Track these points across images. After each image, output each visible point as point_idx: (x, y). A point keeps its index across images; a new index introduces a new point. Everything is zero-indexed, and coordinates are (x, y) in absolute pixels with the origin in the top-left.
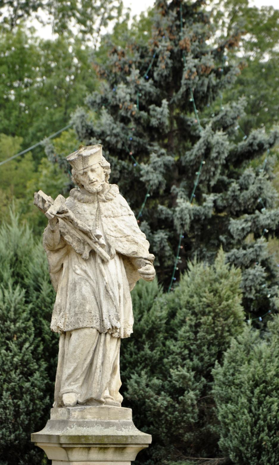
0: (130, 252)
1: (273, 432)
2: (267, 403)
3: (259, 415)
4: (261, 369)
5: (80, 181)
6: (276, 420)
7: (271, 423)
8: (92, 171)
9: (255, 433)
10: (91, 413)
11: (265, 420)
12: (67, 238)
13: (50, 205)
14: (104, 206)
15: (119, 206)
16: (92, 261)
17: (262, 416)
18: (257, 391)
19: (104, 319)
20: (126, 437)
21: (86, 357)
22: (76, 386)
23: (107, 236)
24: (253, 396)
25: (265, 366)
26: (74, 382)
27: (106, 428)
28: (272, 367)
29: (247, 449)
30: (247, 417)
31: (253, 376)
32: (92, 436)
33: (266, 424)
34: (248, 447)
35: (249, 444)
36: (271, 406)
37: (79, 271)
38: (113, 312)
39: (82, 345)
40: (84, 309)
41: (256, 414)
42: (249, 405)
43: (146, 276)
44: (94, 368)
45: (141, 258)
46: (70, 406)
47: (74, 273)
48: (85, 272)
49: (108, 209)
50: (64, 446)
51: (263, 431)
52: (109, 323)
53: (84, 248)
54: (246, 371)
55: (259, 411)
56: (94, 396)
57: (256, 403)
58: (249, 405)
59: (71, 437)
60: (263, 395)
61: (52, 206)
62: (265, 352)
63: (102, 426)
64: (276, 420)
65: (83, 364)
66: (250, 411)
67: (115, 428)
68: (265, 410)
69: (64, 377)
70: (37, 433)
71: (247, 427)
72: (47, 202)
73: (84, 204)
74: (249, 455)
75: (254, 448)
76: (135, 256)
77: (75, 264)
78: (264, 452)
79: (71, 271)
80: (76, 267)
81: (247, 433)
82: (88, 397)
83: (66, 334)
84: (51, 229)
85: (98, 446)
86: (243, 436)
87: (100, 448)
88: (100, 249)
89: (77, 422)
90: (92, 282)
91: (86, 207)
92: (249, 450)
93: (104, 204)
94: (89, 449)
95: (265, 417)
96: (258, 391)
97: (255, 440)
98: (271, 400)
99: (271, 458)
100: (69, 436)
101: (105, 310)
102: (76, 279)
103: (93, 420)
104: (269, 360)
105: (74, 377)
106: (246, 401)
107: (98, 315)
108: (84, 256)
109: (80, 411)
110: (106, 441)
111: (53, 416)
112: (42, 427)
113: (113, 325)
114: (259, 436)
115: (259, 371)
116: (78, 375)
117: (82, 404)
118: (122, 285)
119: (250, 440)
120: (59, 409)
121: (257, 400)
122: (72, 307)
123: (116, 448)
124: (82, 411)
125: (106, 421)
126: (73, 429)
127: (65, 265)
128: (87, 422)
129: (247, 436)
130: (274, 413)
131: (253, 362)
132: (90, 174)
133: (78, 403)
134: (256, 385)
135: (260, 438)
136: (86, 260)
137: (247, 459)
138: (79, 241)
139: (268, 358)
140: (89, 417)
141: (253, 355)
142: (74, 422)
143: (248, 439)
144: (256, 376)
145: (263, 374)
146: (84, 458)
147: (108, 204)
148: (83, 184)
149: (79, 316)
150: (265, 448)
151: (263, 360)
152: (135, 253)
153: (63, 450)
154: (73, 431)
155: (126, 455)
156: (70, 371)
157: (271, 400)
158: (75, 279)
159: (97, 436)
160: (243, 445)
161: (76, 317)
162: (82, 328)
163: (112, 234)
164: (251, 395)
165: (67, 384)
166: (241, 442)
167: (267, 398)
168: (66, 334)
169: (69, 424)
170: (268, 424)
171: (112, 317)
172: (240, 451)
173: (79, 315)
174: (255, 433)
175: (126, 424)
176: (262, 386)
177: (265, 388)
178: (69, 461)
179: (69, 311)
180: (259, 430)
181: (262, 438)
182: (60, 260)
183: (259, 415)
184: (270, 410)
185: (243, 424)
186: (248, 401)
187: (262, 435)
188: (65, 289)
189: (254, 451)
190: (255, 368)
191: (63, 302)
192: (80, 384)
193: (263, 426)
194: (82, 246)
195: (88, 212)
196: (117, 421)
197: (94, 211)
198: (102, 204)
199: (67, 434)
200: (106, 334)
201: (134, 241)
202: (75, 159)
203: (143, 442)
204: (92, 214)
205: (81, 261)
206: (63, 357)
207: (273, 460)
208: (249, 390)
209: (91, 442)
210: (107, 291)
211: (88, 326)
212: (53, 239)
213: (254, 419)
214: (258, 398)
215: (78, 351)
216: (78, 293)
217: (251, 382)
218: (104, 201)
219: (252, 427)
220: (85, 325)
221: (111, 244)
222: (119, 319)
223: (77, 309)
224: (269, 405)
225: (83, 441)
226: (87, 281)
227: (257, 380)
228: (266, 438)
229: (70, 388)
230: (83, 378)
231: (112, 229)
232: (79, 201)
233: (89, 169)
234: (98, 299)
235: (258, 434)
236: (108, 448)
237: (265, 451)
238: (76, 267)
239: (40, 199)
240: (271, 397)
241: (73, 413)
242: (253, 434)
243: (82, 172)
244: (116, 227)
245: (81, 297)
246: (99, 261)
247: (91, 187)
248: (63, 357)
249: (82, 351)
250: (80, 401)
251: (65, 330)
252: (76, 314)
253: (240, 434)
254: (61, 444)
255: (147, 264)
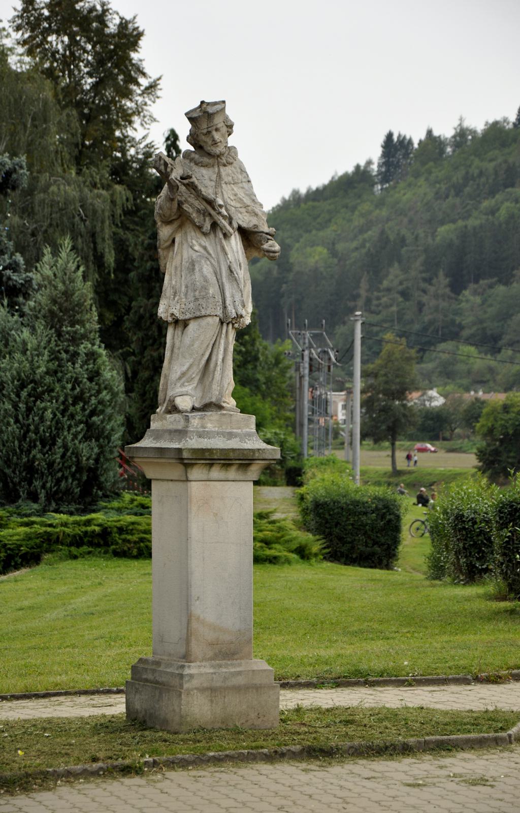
0: (251, 225)
1: (47, 448)
2: (39, 409)
3: (29, 425)
4: (28, 365)
5: (198, 141)
6: (51, 431)
7: (45, 435)
8: (217, 130)
9: (25, 449)
10: (211, 421)
11: (36, 432)
12: (186, 207)
13: (172, 169)
14: (225, 171)
15: (239, 171)
16: (212, 236)
17: (32, 427)
18: (24, 394)
19: (227, 305)
20: (253, 451)
21: (205, 352)
22: (190, 388)
23: (228, 206)
24: (20, 401)
25: (32, 361)
26: (188, 382)
27: (228, 439)
28: (41, 362)
29: (14, 472)
30: (13, 428)
31: (18, 373)
32: (216, 449)
33: (38, 438)
34: (15, 469)
35: (17, 464)
36: (43, 413)
37: (197, 248)
38: (238, 298)
39: (202, 338)
40: (207, 293)
41: (24, 424)
42: (15, 413)
43: (271, 254)
44: (212, 365)
45: (263, 232)
46: (187, 412)
47: (190, 250)
48: (205, 248)
49: (228, 175)
50: (186, 461)
51: (35, 446)
52: (234, 311)
53: (205, 220)
54: (8, 367)
55: (27, 420)
56: (214, 400)
57: (24, 410)
58: (15, 413)
59: (195, 451)
60: (32, 399)
61: (174, 170)
62: (31, 342)
63: (224, 437)
64: (51, 431)
65: (200, 360)
66: (17, 421)
67: (238, 439)
68: (36, 418)
69: (174, 376)
70: (135, 445)
71: (14, 443)
72: (169, 165)
73: (202, 168)
74: (17, 480)
75: (24, 470)
76: (256, 230)
77: (192, 239)
78: (36, 476)
79: (185, 246)
80: (194, 242)
81: (15, 450)
82: (207, 400)
83: (181, 324)
84: (171, 197)
85: (222, 462)
86: (9, 455)
87: (224, 465)
88: (223, 221)
89: (197, 431)
90: (213, 261)
91: (204, 171)
92: (17, 472)
93: (225, 168)
94: (211, 465)
95: (37, 428)
96: (26, 394)
97: (25, 460)
98: (43, 405)
99: (47, 482)
100: (192, 449)
101: (228, 294)
102: (194, 257)
103: (213, 429)
104: (36, 352)
105: (187, 376)
106: (10, 407)
107: (221, 301)
108: (204, 230)
109: (200, 418)
110: (232, 455)
111: (154, 425)
112: (138, 439)
113: (239, 313)
114: (30, 453)
115: (24, 367)
116: (193, 373)
117: (198, 410)
118: (242, 265)
119: (18, 459)
120: (168, 416)
121: (25, 406)
122: (189, 291)
123: (241, 464)
124: (202, 418)
125: (227, 431)
126: (194, 440)
127: (177, 240)
128: (207, 432)
129: (15, 453)
130: (49, 423)
131: (18, 356)
132: (214, 133)
133: (194, 409)
134: (23, 386)
135: (31, 456)
136: (205, 234)
137: (15, 484)
138: (198, 211)
139: (35, 350)
140: (210, 426)
141: (13, 346)
142: (193, 432)
143: (15, 457)
144: (23, 374)
145: (31, 371)
146: (205, 478)
147: (229, 169)
148: (202, 144)
149: (201, 301)
150: (38, 470)
151: (28, 353)
152: (256, 226)
153: (182, 467)
154: (194, 443)
155: (249, 474)
156: (184, 368)
157: (43, 405)
158: (192, 257)
159: (222, 449)
160: (9, 467)
161: (198, 303)
162: (205, 316)
163: (232, 203)
164: (18, 399)
165: (179, 385)
166: (5, 462)
167: (38, 402)
168: (181, 324)
169: (188, 435)
170: (40, 437)
171: (237, 303)
172: (5, 474)
173: (200, 300)
174: (25, 449)
175: (249, 435)
176: (30, 386)
177: (34, 389)
178: (187, 480)
179: (186, 295)
180: (30, 446)
181: (34, 456)
182: (172, 233)
183: (29, 425)
184: (42, 419)
185: (8, 438)
186: (13, 407)
187: (34, 452)
188: (179, 269)
189: (24, 474)
190: (20, 363)
191: (178, 284)
192: (195, 385)
193: (35, 441)
194: (202, 218)
195: (206, 177)
196: (239, 431)
197: (214, 177)
198: (222, 169)
199: (189, 447)
200: (228, 324)
201: (254, 212)
202: (199, 116)
203: (271, 457)
204: (211, 180)
205: (199, 235)
206: (172, 351)
207: (48, 485)
208: (13, 392)
209: (216, 457)
210: (231, 271)
211: (212, 314)
212: (171, 209)
213: (22, 431)
214: (26, 404)
215: (197, 344)
216: (197, 276)
217: (16, 382)
218: (225, 165)
219: (20, 442)
220: (208, 313)
221: (232, 216)
222: (244, 306)
223: (197, 293)
224: (41, 412)
225: (207, 455)
226: (208, 259)
227: (23, 379)
228: (39, 456)
229: (184, 389)
230: (198, 378)
231: (232, 198)
232: (196, 164)
233: (214, 128)
234: (220, 281)
235: (29, 451)
236: (232, 464)
237: (38, 474)
238: (194, 242)
239: (162, 162)
240: (42, 401)
241: (193, 421)
242: (22, 451)
243: (205, 131)
244: (236, 195)
245: (202, 279)
246: (221, 236)
247: (214, 149)
248: (172, 351)
249: (202, 344)
250: (197, 405)
251: (181, 317)
252: (196, 299)
253: (4, 451)
254: (182, 459)
255: (269, 239)
